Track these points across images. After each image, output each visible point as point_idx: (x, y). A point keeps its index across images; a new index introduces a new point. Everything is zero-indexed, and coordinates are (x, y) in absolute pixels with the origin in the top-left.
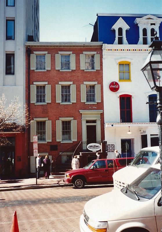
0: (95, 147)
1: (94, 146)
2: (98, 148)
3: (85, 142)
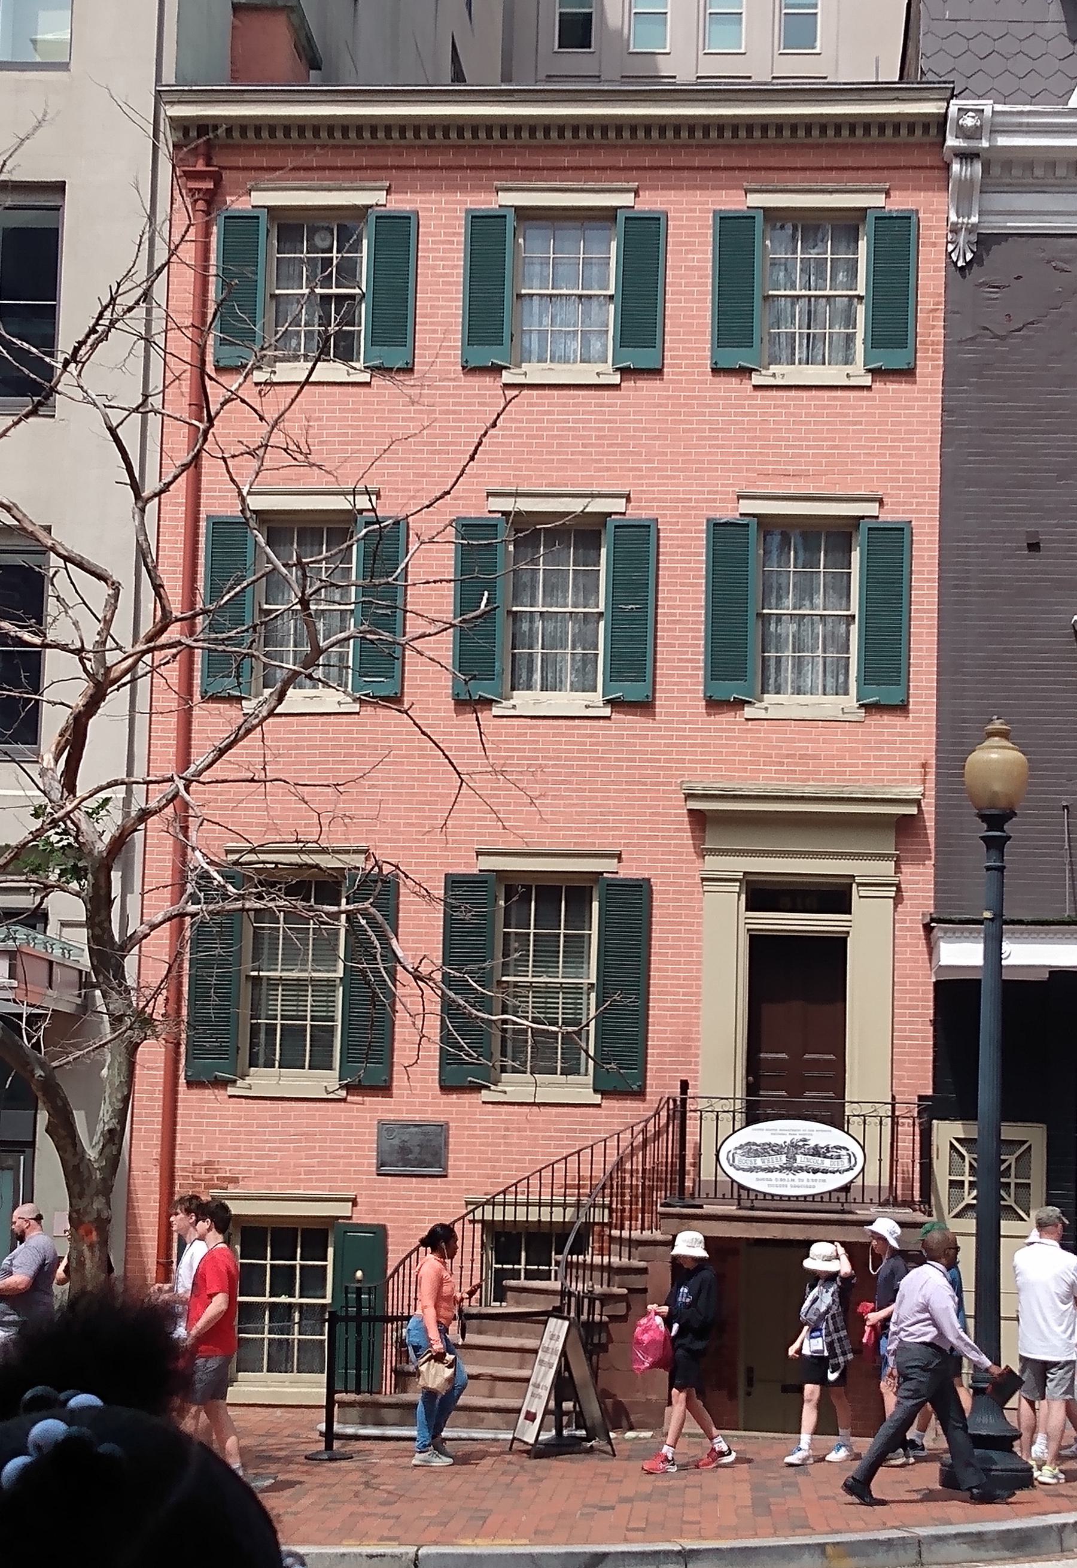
0: (801, 1160)
1: (794, 1148)
2: (827, 1163)
3: (718, 1106)
